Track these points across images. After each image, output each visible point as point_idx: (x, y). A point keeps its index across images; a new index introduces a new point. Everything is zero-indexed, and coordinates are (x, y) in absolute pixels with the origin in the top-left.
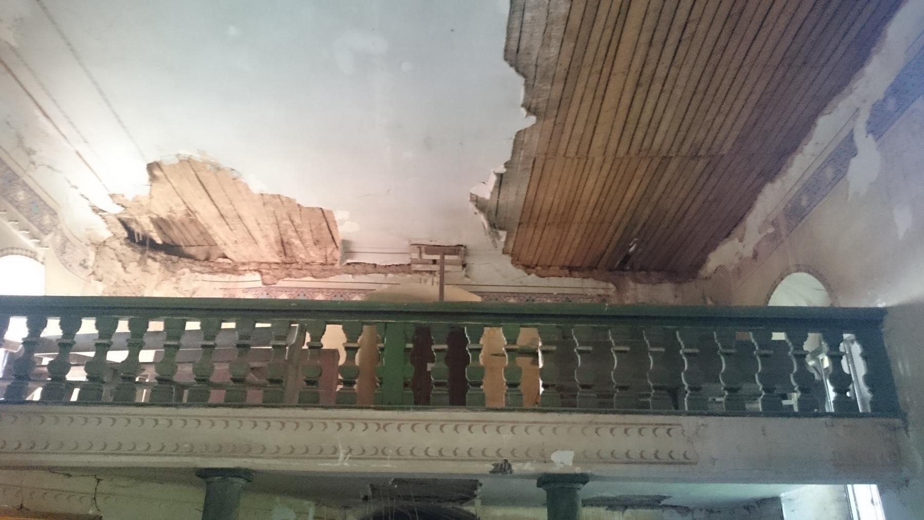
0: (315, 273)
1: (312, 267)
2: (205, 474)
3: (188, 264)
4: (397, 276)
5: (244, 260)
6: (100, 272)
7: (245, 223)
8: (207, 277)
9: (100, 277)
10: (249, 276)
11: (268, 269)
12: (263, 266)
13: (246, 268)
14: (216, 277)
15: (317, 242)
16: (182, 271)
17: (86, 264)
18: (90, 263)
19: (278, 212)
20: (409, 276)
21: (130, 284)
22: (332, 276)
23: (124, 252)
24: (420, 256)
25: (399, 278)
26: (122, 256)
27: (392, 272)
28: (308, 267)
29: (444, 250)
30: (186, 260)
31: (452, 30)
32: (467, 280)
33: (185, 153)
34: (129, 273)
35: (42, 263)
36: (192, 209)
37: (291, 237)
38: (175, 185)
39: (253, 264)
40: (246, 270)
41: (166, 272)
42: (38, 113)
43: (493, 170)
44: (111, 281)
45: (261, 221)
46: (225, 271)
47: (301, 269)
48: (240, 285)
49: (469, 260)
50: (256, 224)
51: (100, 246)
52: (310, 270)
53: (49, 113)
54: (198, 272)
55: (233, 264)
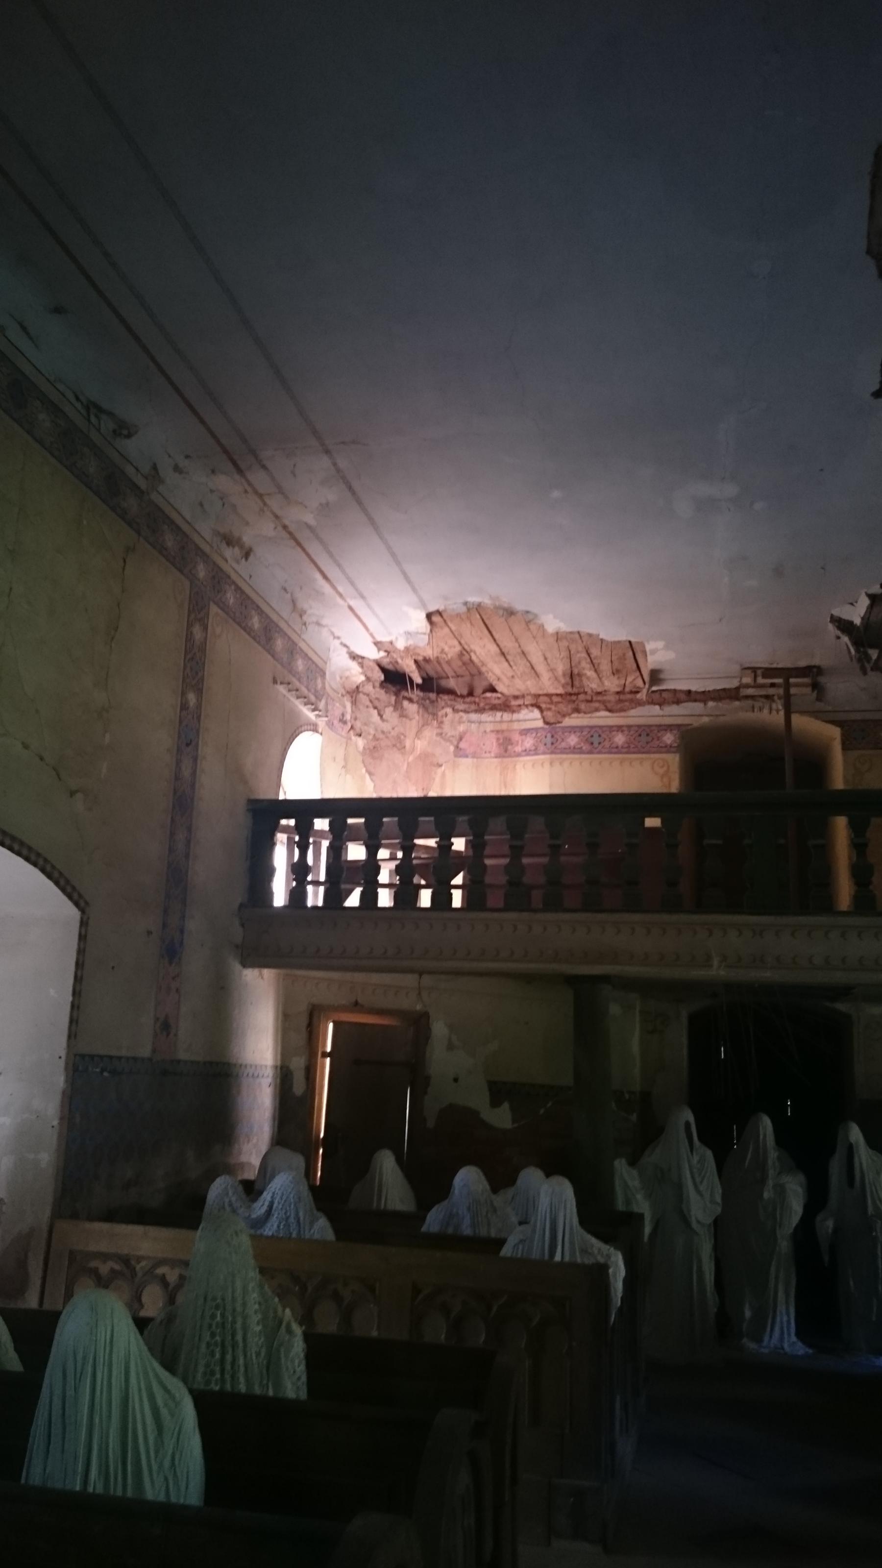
0: (609, 705)
1: (605, 698)
2: (572, 981)
3: (449, 702)
4: (720, 704)
5: (517, 693)
6: (358, 725)
7: (529, 658)
8: (474, 716)
9: (358, 731)
10: (525, 714)
11: (549, 703)
12: (542, 699)
13: (520, 702)
14: (485, 717)
15: (616, 672)
16: (443, 712)
18: (348, 717)
19: (573, 648)
20: (737, 703)
22: (632, 708)
23: (377, 696)
24: (755, 680)
25: (724, 705)
27: (713, 699)
28: (600, 698)
29: (787, 673)
30: (446, 697)
32: (820, 706)
33: (474, 599)
34: (387, 721)
35: (321, 734)
36: (468, 650)
37: (584, 669)
38: (453, 628)
39: (529, 697)
40: (520, 706)
41: (426, 715)
42: (318, 576)
43: (866, 590)
44: (369, 734)
45: (548, 655)
46: (494, 708)
47: (591, 701)
48: (516, 726)
49: (822, 680)
50: (542, 659)
51: (354, 693)
52: (603, 702)
53: (329, 575)
54: (461, 711)
55: (503, 699)
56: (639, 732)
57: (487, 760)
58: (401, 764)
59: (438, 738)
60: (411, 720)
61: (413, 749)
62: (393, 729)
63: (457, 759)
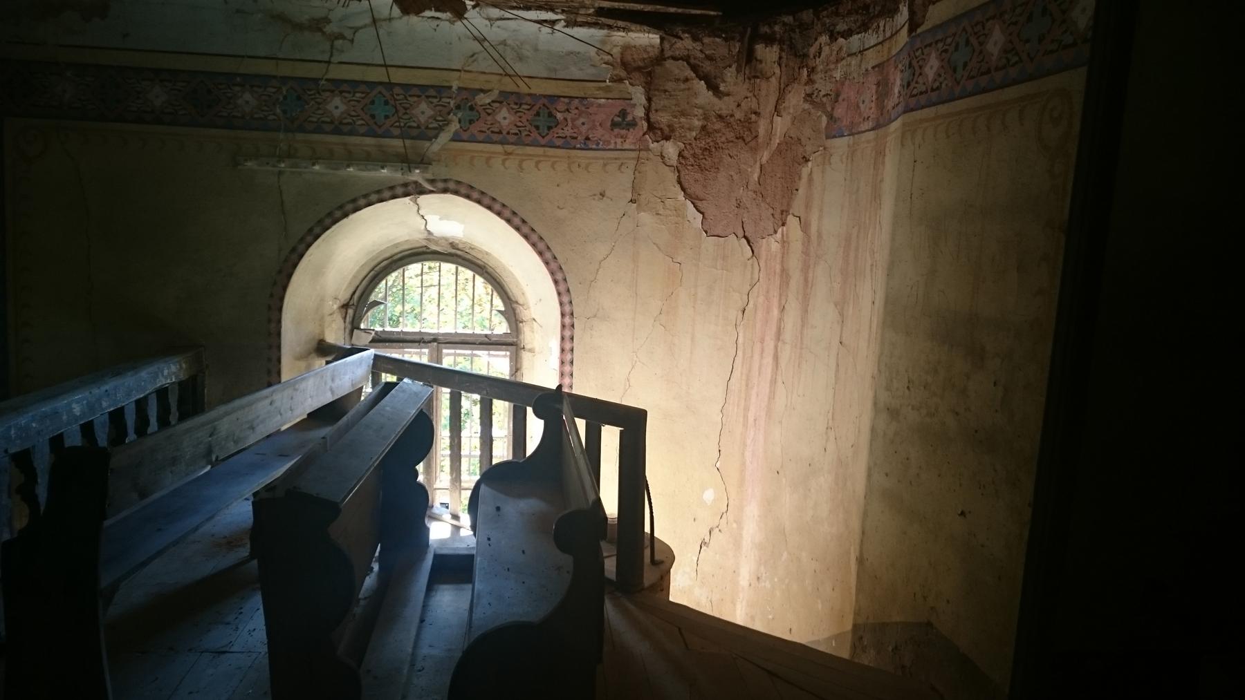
17: (629, 118)
21: (732, 120)
26: (708, 63)
56: (536, 108)
58: (749, 170)
59: (807, 106)
61: (770, 135)
62: (739, 105)
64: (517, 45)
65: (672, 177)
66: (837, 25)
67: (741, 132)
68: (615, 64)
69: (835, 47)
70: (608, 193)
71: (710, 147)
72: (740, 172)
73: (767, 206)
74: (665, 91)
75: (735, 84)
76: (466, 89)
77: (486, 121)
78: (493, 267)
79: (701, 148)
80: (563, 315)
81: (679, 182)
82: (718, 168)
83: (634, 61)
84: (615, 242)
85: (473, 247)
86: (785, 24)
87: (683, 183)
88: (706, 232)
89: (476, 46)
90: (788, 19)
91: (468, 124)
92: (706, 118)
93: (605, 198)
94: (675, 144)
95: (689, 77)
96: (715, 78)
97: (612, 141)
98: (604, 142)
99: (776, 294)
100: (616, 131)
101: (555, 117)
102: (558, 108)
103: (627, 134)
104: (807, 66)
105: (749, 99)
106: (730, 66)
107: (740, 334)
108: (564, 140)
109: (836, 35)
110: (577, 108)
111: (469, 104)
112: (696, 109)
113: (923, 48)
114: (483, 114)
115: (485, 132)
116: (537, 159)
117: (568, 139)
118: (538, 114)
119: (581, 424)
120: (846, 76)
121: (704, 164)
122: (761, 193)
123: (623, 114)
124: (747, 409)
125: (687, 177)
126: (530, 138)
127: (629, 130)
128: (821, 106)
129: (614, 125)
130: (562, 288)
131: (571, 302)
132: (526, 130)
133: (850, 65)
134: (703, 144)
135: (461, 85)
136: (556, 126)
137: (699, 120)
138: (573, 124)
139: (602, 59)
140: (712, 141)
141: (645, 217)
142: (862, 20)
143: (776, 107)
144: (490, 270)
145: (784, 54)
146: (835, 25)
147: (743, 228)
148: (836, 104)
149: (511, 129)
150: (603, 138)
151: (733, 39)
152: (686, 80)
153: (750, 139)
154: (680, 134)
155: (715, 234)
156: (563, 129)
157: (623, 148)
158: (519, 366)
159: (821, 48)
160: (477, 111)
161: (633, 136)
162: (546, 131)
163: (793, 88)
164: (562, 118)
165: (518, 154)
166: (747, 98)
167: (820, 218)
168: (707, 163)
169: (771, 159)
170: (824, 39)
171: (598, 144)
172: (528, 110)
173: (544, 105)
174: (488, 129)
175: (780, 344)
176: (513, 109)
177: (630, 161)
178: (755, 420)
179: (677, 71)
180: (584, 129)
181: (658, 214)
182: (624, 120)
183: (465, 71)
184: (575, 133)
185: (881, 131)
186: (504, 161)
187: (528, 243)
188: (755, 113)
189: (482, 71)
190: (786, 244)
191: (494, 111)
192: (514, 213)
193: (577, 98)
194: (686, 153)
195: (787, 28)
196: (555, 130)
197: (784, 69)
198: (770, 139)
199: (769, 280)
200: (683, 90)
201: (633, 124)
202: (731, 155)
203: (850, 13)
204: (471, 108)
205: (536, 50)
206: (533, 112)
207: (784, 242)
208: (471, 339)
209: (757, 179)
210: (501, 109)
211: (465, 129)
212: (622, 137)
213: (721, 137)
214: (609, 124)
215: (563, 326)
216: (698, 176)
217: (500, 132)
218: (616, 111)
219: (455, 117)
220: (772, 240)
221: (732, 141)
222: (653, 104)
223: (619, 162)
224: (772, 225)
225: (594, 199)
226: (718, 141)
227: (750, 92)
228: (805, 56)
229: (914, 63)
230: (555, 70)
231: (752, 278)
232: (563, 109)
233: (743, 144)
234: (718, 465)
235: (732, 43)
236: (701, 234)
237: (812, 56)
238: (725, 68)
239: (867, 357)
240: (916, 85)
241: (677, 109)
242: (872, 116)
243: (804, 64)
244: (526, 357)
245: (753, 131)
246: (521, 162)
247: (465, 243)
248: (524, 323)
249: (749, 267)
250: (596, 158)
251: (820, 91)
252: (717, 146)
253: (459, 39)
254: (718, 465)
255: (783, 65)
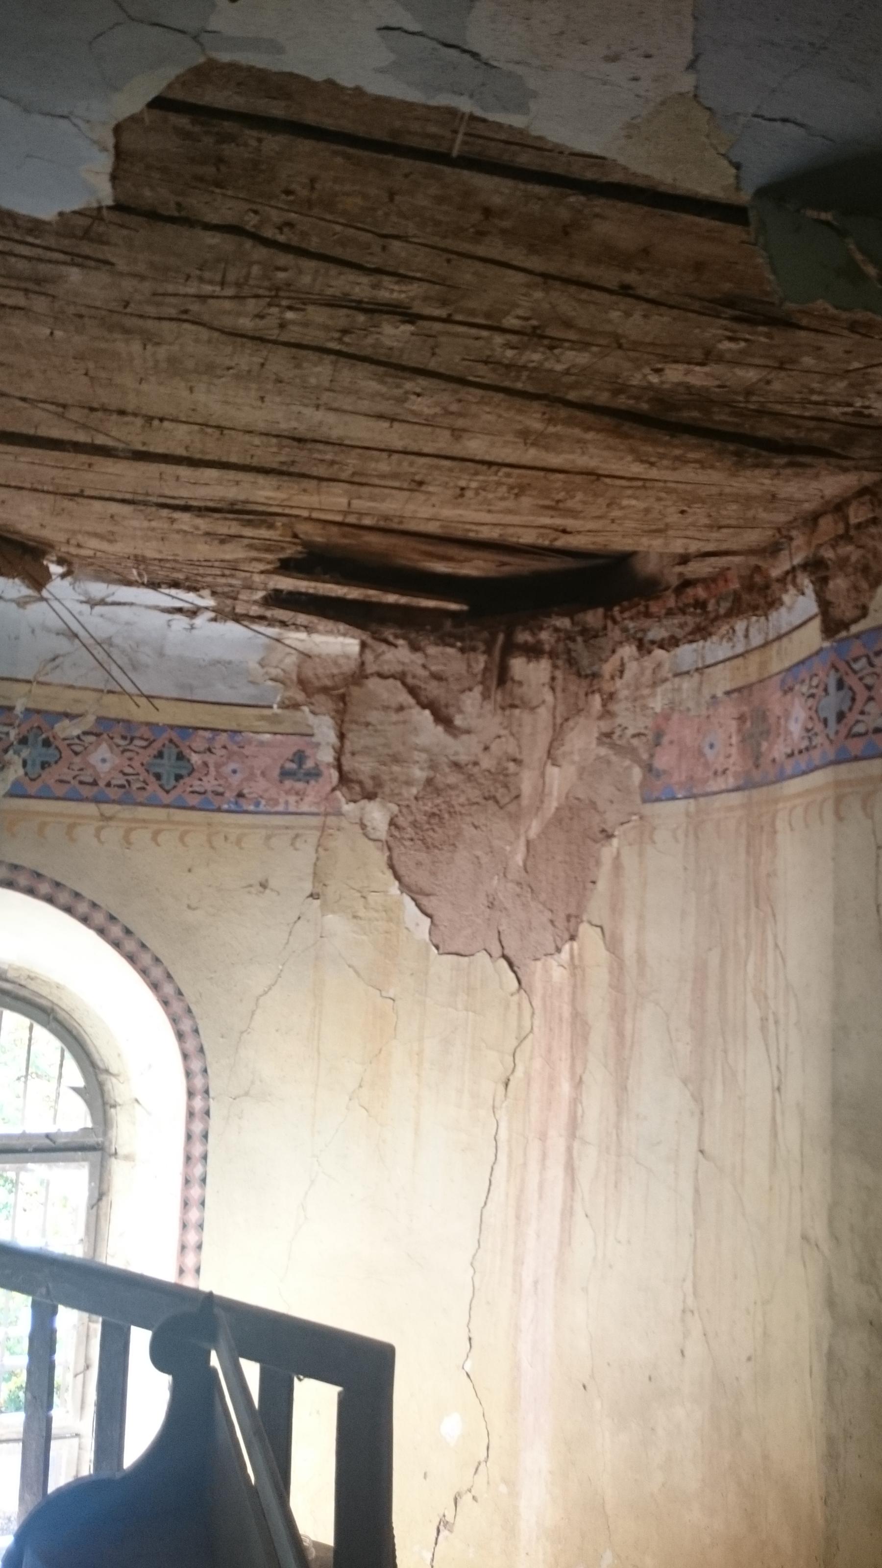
16: (614, 661)
17: (309, 764)
21: (476, 770)
26: (434, 683)
31: (25, 1210)
56: (157, 745)
57: (719, 801)
58: (508, 848)
59: (603, 751)
60: (533, 709)
61: (541, 794)
62: (486, 749)
63: (649, 809)
64: (130, 646)
65: (379, 858)
66: (649, 630)
67: (492, 789)
68: (288, 682)
69: (648, 663)
70: (272, 883)
71: (440, 810)
72: (492, 852)
73: (541, 907)
74: (368, 724)
75: (480, 716)
76: (38, 712)
77: (71, 764)
78: (67, 1009)
79: (425, 813)
80: (191, 1094)
81: (392, 867)
82: (454, 845)
83: (318, 678)
84: (283, 965)
85: (32, 975)
86: (557, 630)
87: (397, 867)
88: (437, 947)
89: (63, 645)
90: (564, 623)
91: (38, 768)
92: (433, 766)
93: (268, 891)
94: (384, 806)
95: (405, 704)
96: (447, 706)
97: (281, 800)
98: (269, 800)
99: (565, 1055)
100: (288, 783)
101: (189, 761)
102: (194, 746)
103: (305, 789)
104: (599, 690)
105: (503, 739)
106: (470, 689)
107: (503, 1125)
108: (203, 796)
109: (647, 645)
110: (225, 747)
111: (44, 736)
112: (416, 753)
113: (871, 655)
114: (66, 753)
115: (68, 782)
116: (156, 827)
117: (210, 796)
118: (160, 755)
119: (251, 1371)
120: (672, 707)
121: (431, 837)
122: (530, 887)
123: (300, 757)
124: (519, 1261)
125: (403, 858)
126: (145, 794)
127: (308, 782)
128: (630, 752)
129: (285, 774)
130: (191, 1045)
131: (205, 1071)
132: (138, 780)
133: (679, 690)
134: (428, 807)
135: (31, 705)
136: (189, 774)
137: (422, 769)
138: (217, 772)
139: (267, 673)
140: (444, 802)
141: (334, 922)
142: (695, 623)
143: (549, 752)
144: (61, 1015)
145: (559, 674)
146: (645, 631)
147: (500, 941)
148: (658, 748)
149: (113, 778)
150: (266, 795)
151: (474, 649)
152: (401, 708)
153: (507, 799)
154: (392, 790)
155: (453, 950)
156: (200, 780)
157: (300, 811)
158: (105, 1187)
159: (623, 664)
160: (57, 748)
161: (314, 792)
162: (173, 782)
163: (577, 723)
164: (200, 762)
165: (122, 820)
166: (499, 737)
167: (641, 929)
168: (435, 836)
169: (544, 833)
170: (628, 651)
171: (257, 804)
172: (145, 748)
173: (171, 741)
174: (74, 778)
175: (576, 1145)
176: (118, 746)
177: (308, 832)
178: (536, 1283)
179: (385, 695)
180: (235, 780)
181: (355, 917)
182: (300, 765)
183: (39, 683)
184: (220, 785)
185: (757, 794)
186: (98, 831)
187: (135, 968)
188: (514, 760)
189: (70, 683)
190: (578, 972)
191: (86, 748)
192: (112, 918)
193: (225, 731)
194: (401, 821)
195: (562, 635)
196: (187, 780)
197: (559, 694)
198: (542, 802)
199: (551, 1030)
200: (395, 723)
201: (315, 774)
202: (476, 823)
203: (670, 613)
204: (47, 743)
205: (161, 654)
206: (152, 751)
207: (575, 967)
208: (19, 1144)
209: (521, 863)
210: (99, 744)
211: (33, 777)
212: (297, 793)
213: (458, 796)
214: (276, 772)
215: (191, 1114)
216: (423, 856)
217: (95, 783)
218: (289, 753)
219: (16, 757)
220: (552, 962)
221: (477, 803)
222: (347, 744)
223: (291, 833)
224: (551, 938)
225: (249, 893)
226: (454, 803)
227: (505, 728)
228: (595, 676)
229: (851, 680)
230: (191, 688)
231: (520, 1027)
232: (202, 749)
233: (496, 808)
234: (468, 1367)
235: (472, 655)
236: (428, 950)
237: (607, 676)
238: (463, 691)
239: (771, 1189)
240: (861, 717)
241: (386, 751)
242: (732, 769)
243: (595, 688)
244: (118, 1169)
245: (512, 788)
246: (128, 832)
247: (18, 969)
248: (118, 1108)
249: (514, 1007)
250: (254, 826)
251: (626, 728)
252: (452, 810)
253: (33, 631)
254: (468, 1367)
255: (559, 689)
